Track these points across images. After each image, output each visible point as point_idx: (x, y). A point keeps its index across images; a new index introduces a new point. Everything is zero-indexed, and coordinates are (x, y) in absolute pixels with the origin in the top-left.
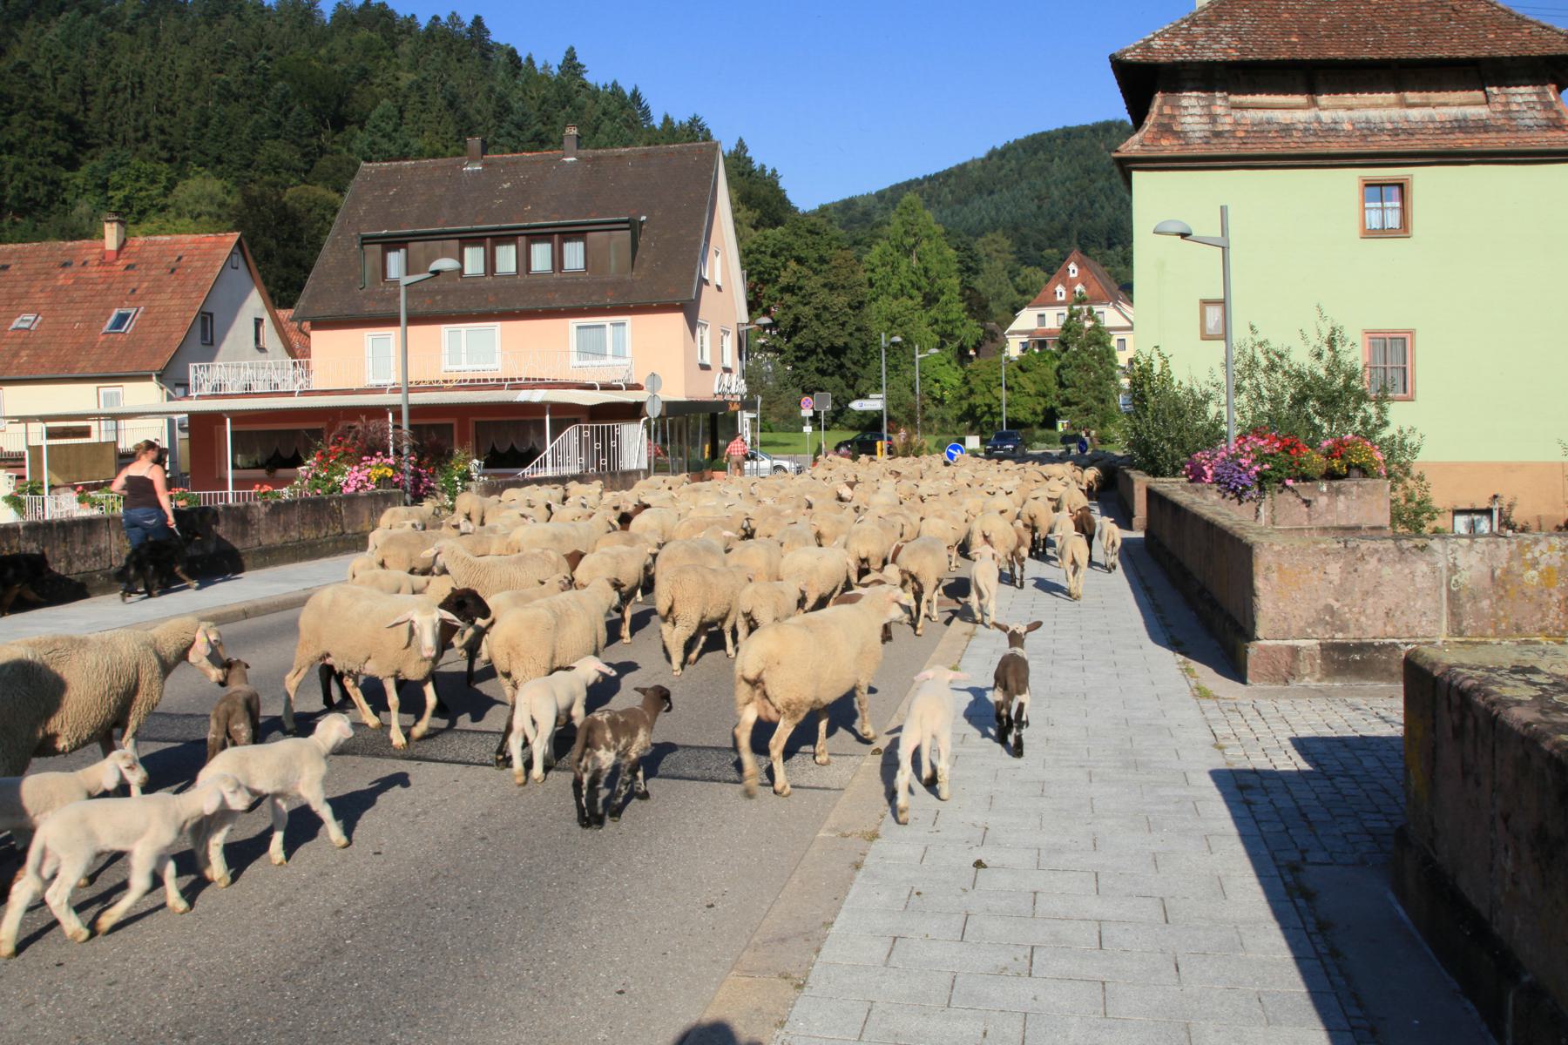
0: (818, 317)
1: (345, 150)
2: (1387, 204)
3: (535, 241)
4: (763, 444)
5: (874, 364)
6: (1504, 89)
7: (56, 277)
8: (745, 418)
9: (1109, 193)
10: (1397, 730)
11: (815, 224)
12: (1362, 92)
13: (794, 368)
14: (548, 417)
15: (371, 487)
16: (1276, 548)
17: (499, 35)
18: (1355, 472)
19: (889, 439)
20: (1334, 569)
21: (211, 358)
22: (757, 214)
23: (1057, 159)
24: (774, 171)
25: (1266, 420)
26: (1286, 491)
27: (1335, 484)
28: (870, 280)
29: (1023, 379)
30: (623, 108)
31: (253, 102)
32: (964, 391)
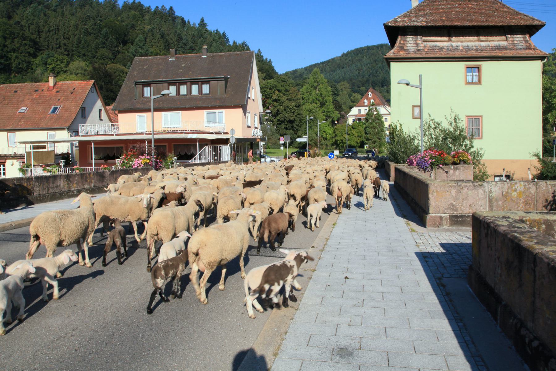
0: (285, 110)
1: (126, 52)
2: (474, 74)
3: (193, 84)
4: (267, 153)
5: (304, 126)
6: (512, 36)
7: (33, 95)
8: (261, 144)
9: (382, 68)
10: (470, 241)
11: (284, 79)
12: (466, 36)
13: (277, 127)
14: (198, 143)
15: (142, 166)
16: (436, 185)
17: (178, 13)
18: (462, 163)
19: (309, 151)
20: (454, 192)
21: (85, 123)
22: (265, 75)
23: (365, 57)
24: (270, 60)
25: (434, 145)
26: (440, 168)
27: (456, 166)
28: (302, 97)
29: (353, 131)
30: (220, 38)
31: (96, 35)
32: (334, 135)
